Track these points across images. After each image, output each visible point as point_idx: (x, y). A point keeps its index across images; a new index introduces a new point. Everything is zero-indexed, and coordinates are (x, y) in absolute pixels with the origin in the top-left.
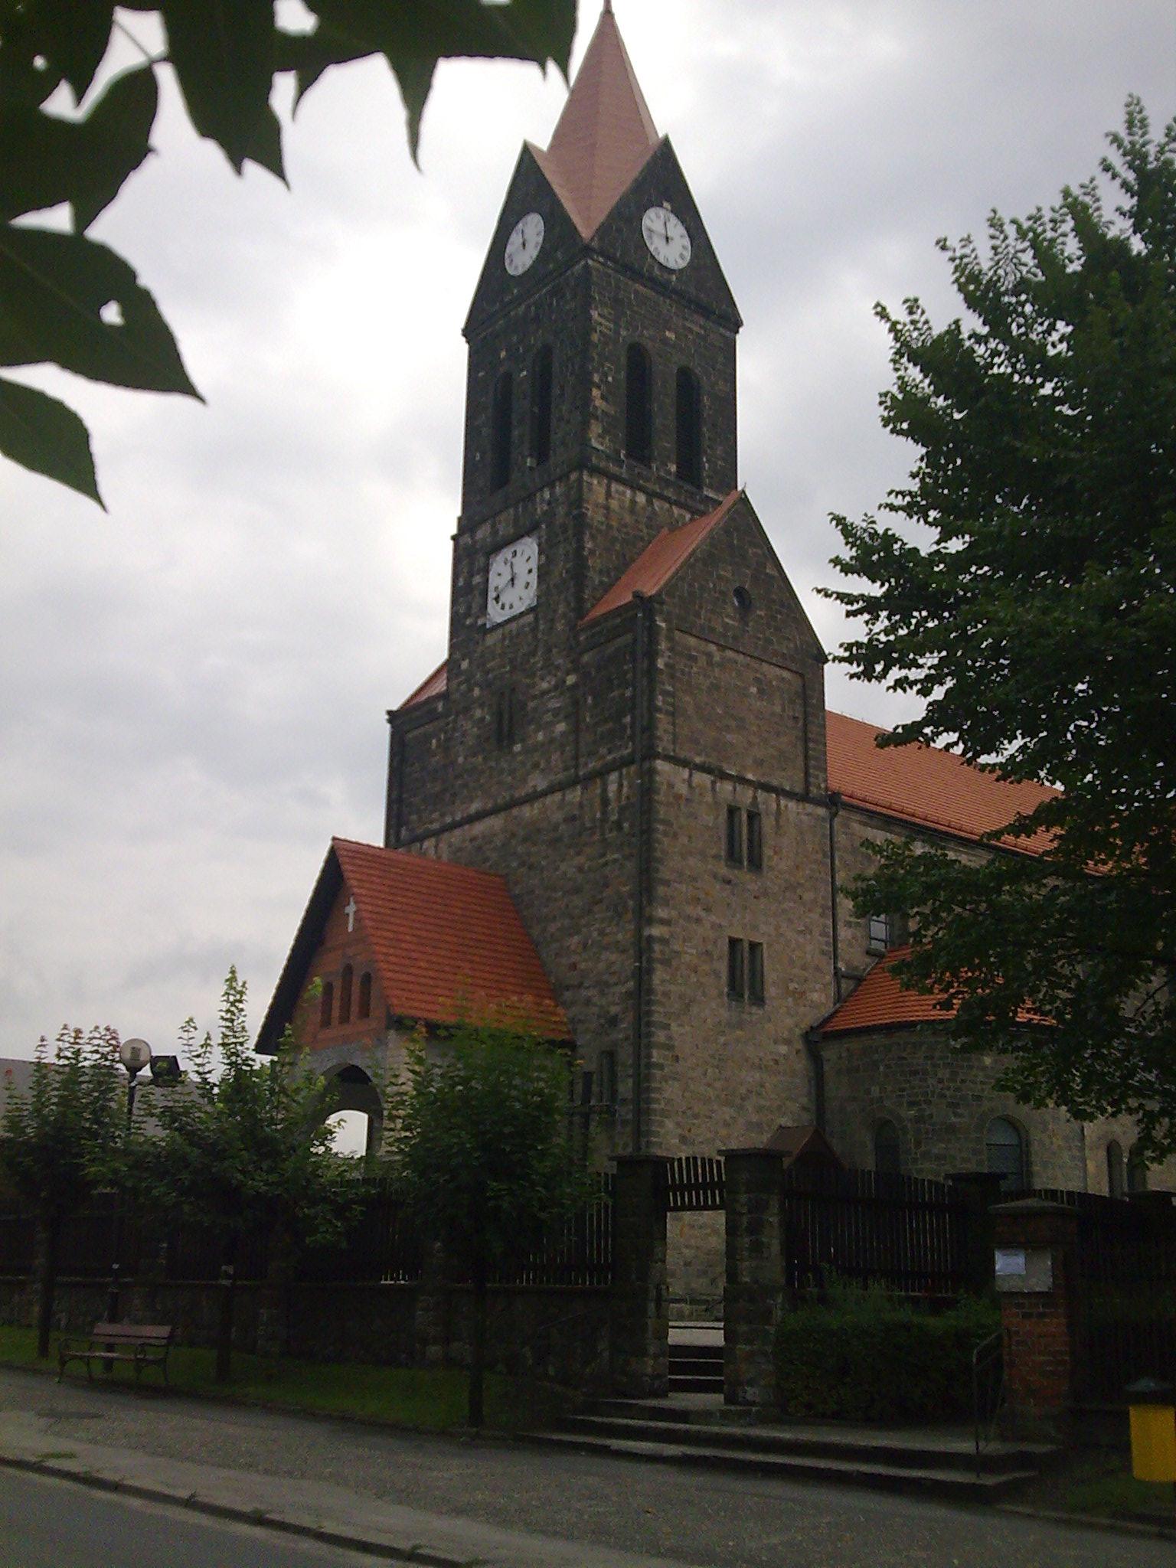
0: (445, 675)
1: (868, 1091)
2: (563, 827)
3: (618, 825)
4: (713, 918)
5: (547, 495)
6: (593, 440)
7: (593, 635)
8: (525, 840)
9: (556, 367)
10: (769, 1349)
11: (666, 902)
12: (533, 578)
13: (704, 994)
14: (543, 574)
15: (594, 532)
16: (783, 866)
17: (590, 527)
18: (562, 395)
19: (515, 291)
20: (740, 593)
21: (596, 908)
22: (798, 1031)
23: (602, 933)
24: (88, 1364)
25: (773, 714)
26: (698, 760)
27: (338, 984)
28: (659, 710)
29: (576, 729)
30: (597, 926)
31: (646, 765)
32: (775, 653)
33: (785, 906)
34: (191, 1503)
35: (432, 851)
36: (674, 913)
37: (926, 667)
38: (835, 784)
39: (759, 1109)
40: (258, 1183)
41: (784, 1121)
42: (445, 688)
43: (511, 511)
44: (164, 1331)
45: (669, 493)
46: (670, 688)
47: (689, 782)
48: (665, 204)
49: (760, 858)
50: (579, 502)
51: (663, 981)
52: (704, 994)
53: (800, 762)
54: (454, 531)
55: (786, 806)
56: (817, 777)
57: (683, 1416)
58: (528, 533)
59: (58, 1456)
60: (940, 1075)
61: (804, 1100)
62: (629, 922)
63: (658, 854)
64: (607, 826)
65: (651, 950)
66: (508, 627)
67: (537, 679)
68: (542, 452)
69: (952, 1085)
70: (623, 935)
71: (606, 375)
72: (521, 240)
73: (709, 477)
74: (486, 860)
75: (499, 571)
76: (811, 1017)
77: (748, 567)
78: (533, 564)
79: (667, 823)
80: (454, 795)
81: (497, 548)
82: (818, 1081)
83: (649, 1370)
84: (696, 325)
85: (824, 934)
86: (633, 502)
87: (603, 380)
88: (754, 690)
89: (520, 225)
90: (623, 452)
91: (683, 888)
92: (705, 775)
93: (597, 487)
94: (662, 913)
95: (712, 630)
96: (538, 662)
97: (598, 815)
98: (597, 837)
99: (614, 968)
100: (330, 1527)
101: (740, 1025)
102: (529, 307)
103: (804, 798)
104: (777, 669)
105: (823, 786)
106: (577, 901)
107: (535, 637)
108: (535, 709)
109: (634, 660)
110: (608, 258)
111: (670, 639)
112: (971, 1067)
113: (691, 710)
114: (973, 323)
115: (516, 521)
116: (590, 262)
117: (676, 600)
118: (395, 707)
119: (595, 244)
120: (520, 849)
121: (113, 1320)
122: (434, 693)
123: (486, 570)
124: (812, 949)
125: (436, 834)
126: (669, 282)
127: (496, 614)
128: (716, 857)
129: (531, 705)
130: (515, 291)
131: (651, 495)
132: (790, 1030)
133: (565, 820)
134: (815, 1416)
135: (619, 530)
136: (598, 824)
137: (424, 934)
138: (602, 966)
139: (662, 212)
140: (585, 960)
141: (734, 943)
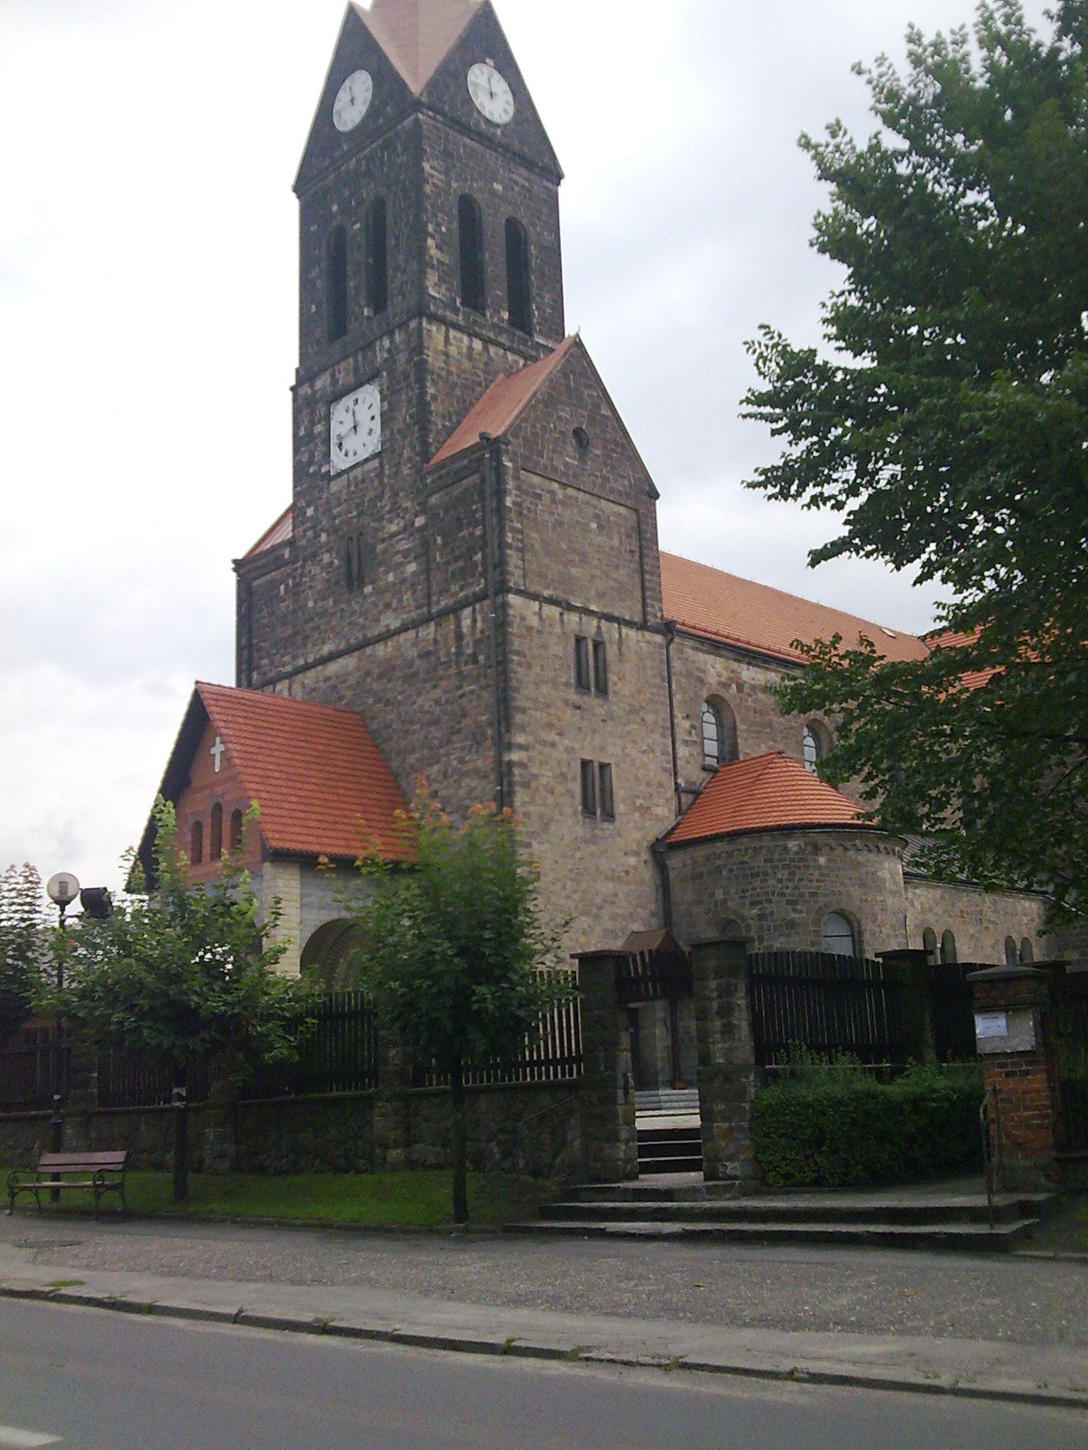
0: (291, 521)
1: (713, 895)
2: (417, 662)
3: (474, 658)
4: (566, 742)
5: (386, 343)
6: (430, 289)
7: (440, 477)
8: (380, 677)
9: (390, 220)
10: (745, 1124)
11: (523, 728)
12: (377, 425)
13: (561, 813)
14: (386, 419)
15: (435, 377)
16: (626, 691)
17: (433, 373)
18: (397, 245)
19: (345, 147)
20: (577, 433)
21: (455, 738)
22: (645, 844)
23: (462, 761)
24: (36, 1194)
25: (612, 548)
26: (546, 593)
27: (207, 822)
28: (510, 546)
29: (426, 570)
30: (457, 755)
31: (499, 599)
32: (612, 491)
33: (630, 728)
34: (239, 1319)
35: (286, 693)
36: (531, 739)
37: (841, 480)
38: (668, 615)
39: (614, 917)
40: (215, 1005)
41: (635, 927)
42: (291, 534)
43: (351, 360)
44: (119, 1156)
45: (503, 339)
46: (519, 525)
47: (539, 614)
48: (488, 60)
49: (606, 685)
50: (419, 349)
51: (524, 803)
52: (561, 813)
53: (638, 594)
54: (293, 382)
55: (627, 635)
56: (653, 607)
57: (668, 1194)
58: (369, 380)
59: (66, 1284)
60: (779, 876)
61: (653, 907)
62: (489, 749)
63: (514, 683)
64: (463, 659)
65: (510, 773)
66: (352, 475)
67: (385, 523)
68: (379, 300)
69: (790, 884)
70: (484, 761)
71: (439, 225)
72: (349, 98)
73: (539, 324)
74: (341, 698)
75: (341, 419)
76: (655, 830)
77: (585, 408)
78: (376, 411)
79: (519, 653)
80: (306, 638)
81: (337, 397)
82: (664, 886)
83: (622, 1155)
84: (521, 176)
85: (664, 753)
86: (470, 348)
87: (437, 230)
88: (594, 526)
89: (347, 83)
90: (458, 301)
91: (538, 714)
92: (554, 607)
93: (436, 333)
94: (520, 739)
95: (555, 469)
96: (385, 506)
97: (453, 650)
98: (453, 671)
99: (475, 793)
100: (406, 1330)
101: (594, 840)
102: (359, 161)
103: (643, 626)
104: (612, 505)
105: (659, 614)
106: (435, 732)
107: (381, 482)
108: (384, 552)
109: (483, 500)
110: (437, 112)
111: (517, 478)
112: (807, 867)
113: (538, 547)
114: (894, 141)
115: (356, 370)
116: (421, 116)
117: (520, 441)
118: (240, 555)
119: (424, 99)
120: (375, 686)
121: (57, 1150)
122: (279, 541)
123: (327, 418)
124: (654, 767)
125: (289, 676)
126: (494, 135)
127: (339, 461)
128: (567, 684)
129: (380, 547)
130: (345, 147)
131: (487, 341)
132: (639, 844)
133: (420, 656)
134: (791, 1185)
135: (459, 376)
136: (453, 658)
137: (292, 770)
138: (462, 792)
139: (485, 69)
140: (446, 788)
141: (585, 764)
